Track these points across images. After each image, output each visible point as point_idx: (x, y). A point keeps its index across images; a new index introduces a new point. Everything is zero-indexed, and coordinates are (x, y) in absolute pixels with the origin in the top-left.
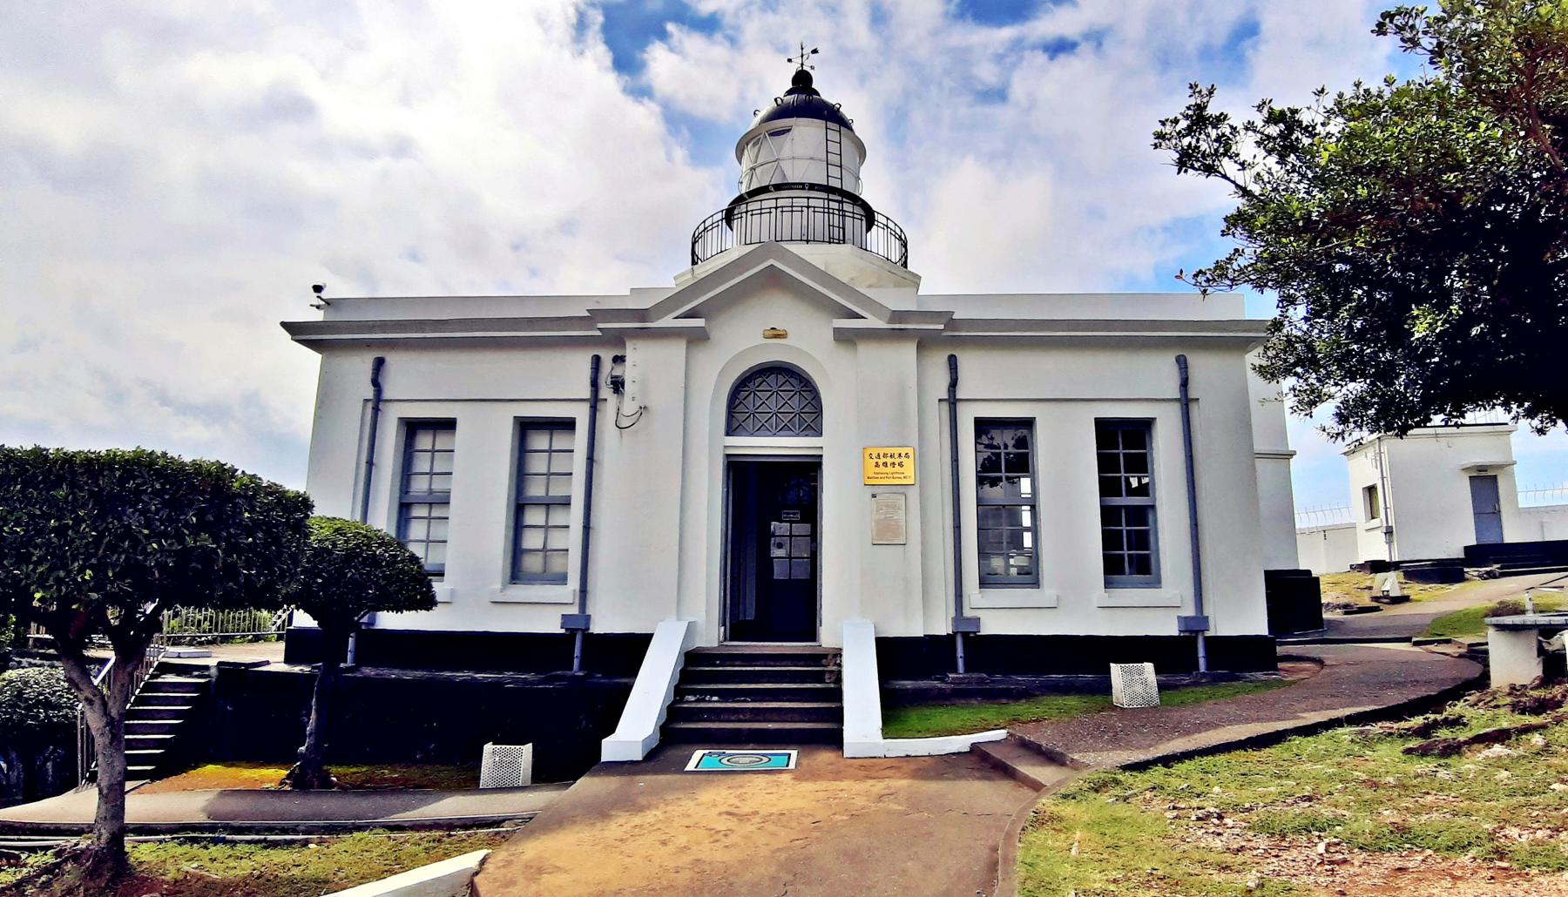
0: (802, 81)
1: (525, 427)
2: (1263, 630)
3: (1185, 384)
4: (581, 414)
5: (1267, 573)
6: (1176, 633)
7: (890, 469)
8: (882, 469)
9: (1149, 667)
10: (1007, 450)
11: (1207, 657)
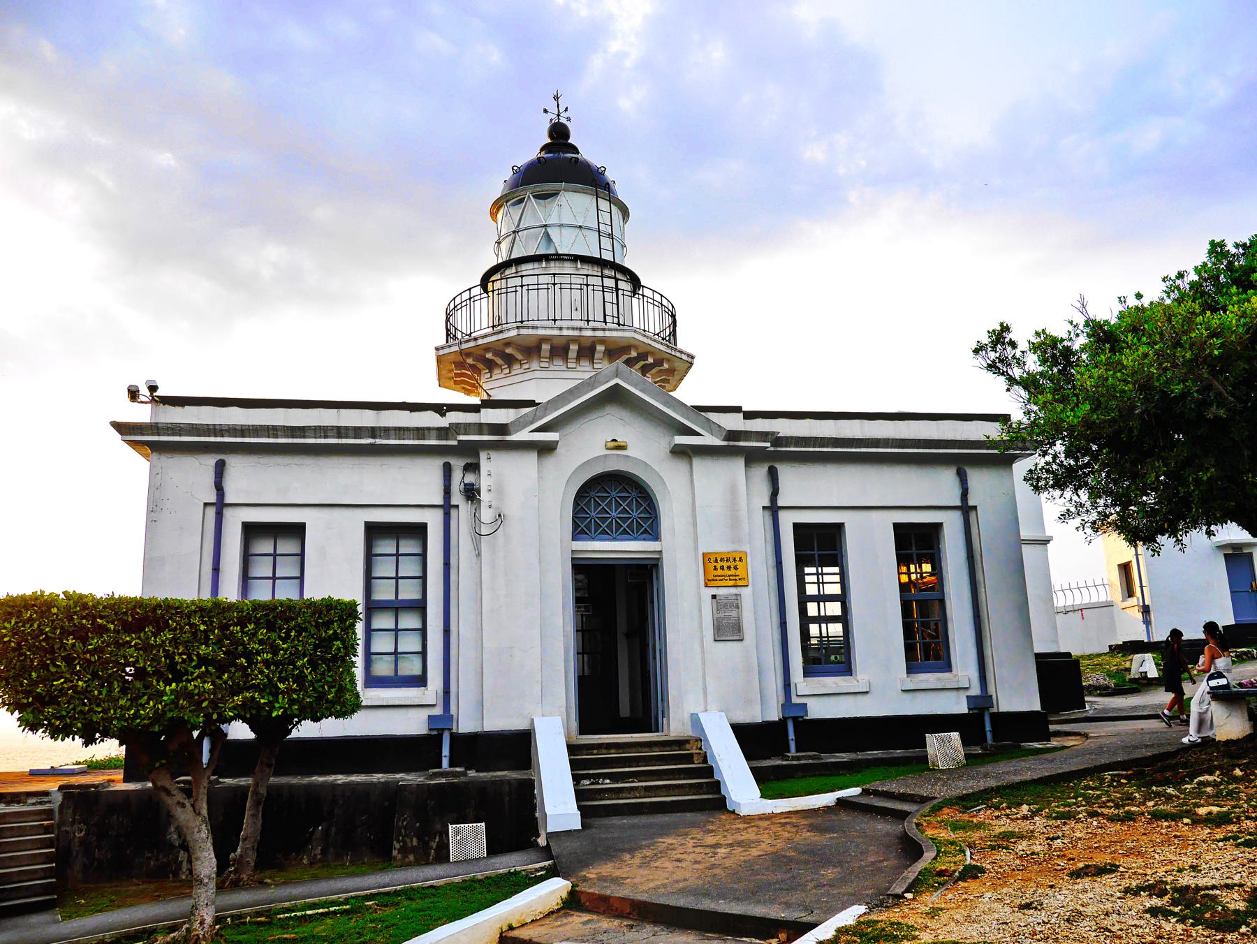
0: (559, 133)
1: (374, 531)
2: (1037, 706)
3: (965, 495)
4: (433, 521)
5: (941, 524)
6: (966, 711)
7: (726, 572)
8: (720, 572)
9: (955, 735)
10: (820, 544)
11: (993, 731)
